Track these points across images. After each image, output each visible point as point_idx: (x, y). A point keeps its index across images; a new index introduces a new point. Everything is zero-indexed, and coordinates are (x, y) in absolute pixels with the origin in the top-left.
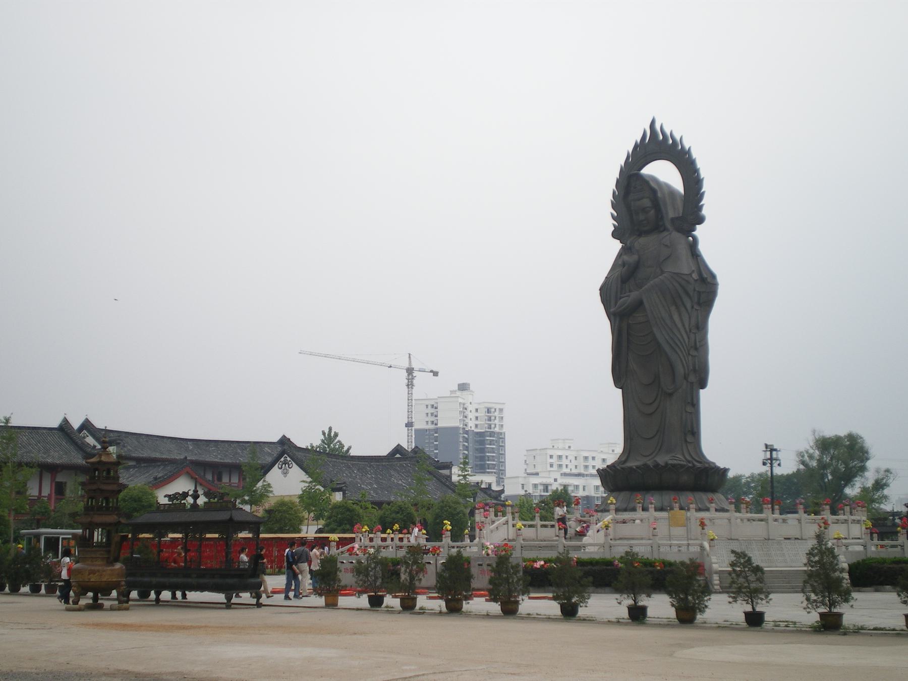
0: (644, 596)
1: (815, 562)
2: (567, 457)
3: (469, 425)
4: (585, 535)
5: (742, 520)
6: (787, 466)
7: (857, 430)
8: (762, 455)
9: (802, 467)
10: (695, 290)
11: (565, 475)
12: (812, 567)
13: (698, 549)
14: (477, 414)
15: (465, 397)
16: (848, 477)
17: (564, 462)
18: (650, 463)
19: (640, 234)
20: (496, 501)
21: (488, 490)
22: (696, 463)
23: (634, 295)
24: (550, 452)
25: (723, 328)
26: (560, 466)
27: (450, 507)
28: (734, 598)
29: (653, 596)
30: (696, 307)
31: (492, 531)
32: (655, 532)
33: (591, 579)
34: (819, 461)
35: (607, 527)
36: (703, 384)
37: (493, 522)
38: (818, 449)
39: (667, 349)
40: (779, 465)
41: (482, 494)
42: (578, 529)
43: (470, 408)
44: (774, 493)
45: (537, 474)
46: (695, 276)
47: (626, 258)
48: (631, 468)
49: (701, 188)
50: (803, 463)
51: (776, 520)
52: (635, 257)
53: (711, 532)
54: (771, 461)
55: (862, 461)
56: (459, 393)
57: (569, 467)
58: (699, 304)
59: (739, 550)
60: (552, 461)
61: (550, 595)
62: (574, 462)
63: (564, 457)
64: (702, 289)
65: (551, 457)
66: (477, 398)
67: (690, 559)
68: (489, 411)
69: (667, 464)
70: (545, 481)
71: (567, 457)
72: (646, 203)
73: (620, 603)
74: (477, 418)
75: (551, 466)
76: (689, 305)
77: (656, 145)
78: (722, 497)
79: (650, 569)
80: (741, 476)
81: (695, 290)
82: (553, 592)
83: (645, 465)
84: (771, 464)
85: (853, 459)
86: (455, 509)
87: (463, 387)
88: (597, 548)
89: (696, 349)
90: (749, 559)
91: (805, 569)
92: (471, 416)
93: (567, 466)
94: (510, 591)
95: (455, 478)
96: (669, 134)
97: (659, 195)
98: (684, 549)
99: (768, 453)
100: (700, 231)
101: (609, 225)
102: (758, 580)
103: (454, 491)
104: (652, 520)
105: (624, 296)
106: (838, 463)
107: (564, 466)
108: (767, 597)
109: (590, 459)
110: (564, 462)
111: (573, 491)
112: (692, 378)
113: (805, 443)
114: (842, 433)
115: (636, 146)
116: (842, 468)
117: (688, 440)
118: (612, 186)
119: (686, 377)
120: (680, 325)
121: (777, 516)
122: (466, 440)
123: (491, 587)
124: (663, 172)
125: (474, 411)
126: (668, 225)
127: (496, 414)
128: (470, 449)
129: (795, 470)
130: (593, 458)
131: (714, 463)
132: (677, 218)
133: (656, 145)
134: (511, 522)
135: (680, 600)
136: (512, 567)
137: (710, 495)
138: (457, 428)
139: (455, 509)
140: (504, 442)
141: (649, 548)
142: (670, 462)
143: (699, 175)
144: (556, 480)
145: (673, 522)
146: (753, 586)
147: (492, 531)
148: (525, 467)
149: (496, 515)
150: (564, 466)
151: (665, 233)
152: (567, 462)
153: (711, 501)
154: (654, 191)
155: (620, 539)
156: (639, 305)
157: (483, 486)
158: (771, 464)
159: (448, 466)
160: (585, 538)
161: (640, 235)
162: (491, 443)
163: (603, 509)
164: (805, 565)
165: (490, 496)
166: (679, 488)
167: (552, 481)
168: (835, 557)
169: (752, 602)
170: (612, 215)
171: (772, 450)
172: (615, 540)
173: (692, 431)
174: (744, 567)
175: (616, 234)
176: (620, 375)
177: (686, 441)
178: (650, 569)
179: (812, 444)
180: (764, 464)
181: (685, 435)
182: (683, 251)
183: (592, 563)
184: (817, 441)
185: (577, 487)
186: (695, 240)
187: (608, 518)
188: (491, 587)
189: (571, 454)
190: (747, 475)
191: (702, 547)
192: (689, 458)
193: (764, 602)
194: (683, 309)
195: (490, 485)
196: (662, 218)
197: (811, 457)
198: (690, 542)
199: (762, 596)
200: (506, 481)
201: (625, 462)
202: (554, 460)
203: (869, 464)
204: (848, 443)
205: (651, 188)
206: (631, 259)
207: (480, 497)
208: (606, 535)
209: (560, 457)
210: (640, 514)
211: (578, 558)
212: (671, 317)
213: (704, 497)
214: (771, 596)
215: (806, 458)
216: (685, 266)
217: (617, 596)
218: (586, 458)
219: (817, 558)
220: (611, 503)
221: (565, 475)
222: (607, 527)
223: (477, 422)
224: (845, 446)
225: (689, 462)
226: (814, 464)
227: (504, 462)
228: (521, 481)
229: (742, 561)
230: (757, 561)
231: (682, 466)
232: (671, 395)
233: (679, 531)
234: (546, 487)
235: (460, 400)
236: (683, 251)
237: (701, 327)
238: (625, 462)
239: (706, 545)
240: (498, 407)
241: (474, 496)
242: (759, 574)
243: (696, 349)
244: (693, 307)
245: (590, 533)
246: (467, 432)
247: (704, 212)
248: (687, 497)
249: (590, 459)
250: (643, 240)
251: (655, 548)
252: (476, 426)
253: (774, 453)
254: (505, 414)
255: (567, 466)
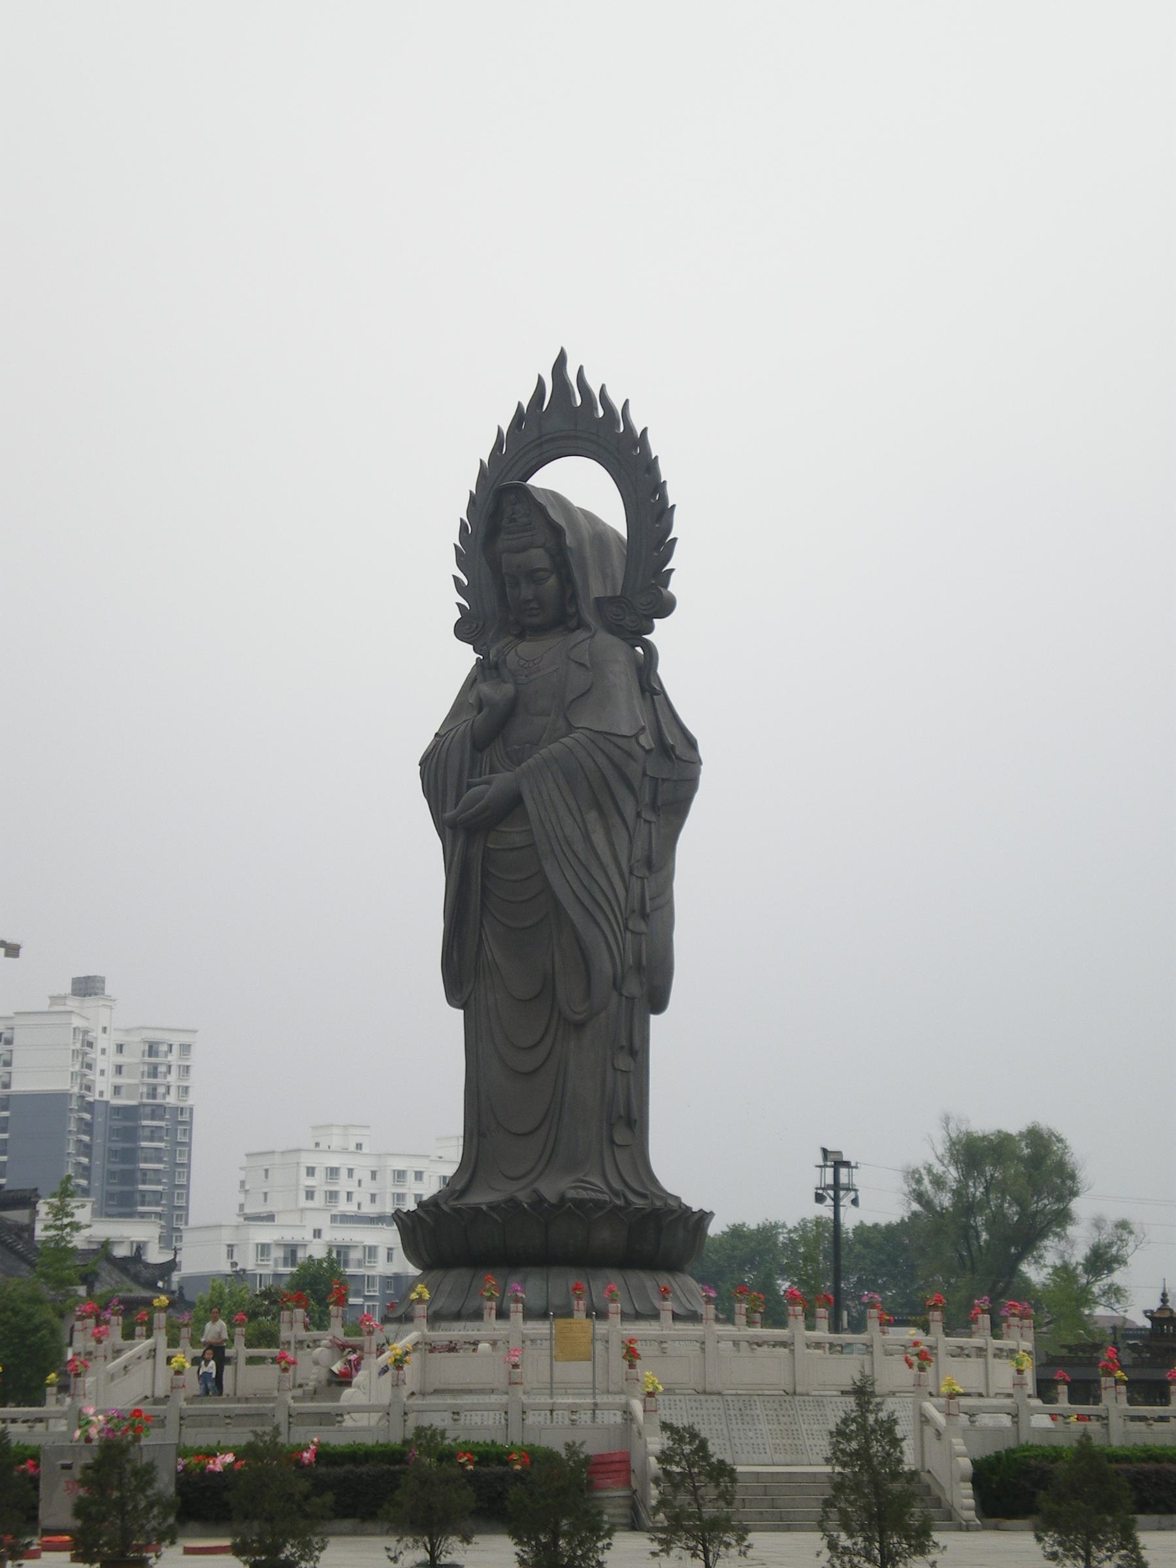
0: (454, 1541)
1: (851, 1455)
2: (351, 1172)
3: (99, 1087)
4: (349, 1384)
5: (736, 1343)
6: (880, 1203)
7: (1049, 1121)
8: (815, 1177)
9: (916, 1207)
10: (644, 774)
11: (345, 1218)
12: (844, 1465)
13: (617, 1418)
14: (120, 1060)
15: (90, 1014)
16: (1027, 1236)
17: (343, 1185)
18: (523, 1197)
19: (523, 633)
20: (137, 1294)
21: (133, 1265)
22: (632, 1197)
23: (502, 780)
24: (308, 1160)
25: (713, 869)
26: (333, 1196)
27: (16, 1312)
28: (661, 1541)
29: (475, 1539)
30: (647, 815)
31: (112, 1377)
32: (524, 1375)
33: (329, 1498)
34: (959, 1194)
35: (399, 1363)
36: (658, 1003)
37: (118, 1352)
38: (955, 1160)
39: (575, 914)
40: (855, 1202)
41: (116, 1275)
42: (337, 1367)
43: (102, 1041)
44: (832, 1275)
45: (270, 1217)
46: (646, 741)
47: (485, 688)
48: (476, 1209)
49: (668, 530)
50: (920, 1197)
51: (818, 1345)
52: (509, 689)
53: (648, 1375)
54: (835, 1191)
55: (1060, 1198)
56: (73, 1004)
57: (356, 1198)
58: (654, 807)
59: (678, 1423)
60: (310, 1182)
61: (227, 1542)
62: (369, 1186)
63: (343, 1173)
64: (660, 773)
65: (311, 1171)
66: (122, 1018)
67: (569, 1447)
68: (152, 1049)
69: (563, 1199)
70: (289, 1236)
71: (351, 1172)
72: (538, 558)
73: (394, 1559)
74: (119, 1069)
75: (310, 1195)
76: (629, 810)
77: (565, 417)
78: (692, 1283)
79: (498, 1469)
80: (776, 1226)
81: (644, 774)
82: (234, 1535)
83: (512, 1201)
84: (836, 1200)
85: (1038, 1193)
86: (30, 1317)
87: (87, 987)
88: (375, 1417)
89: (644, 916)
90: (703, 1445)
91: (828, 1469)
92: (104, 1062)
93: (349, 1195)
94: (127, 1534)
95: (40, 1233)
96: (596, 393)
97: (569, 540)
98: (585, 1417)
99: (830, 1172)
100: (662, 633)
101: (448, 606)
102: (721, 1496)
103: (32, 1265)
104: (515, 1343)
105: (483, 783)
106: (1006, 1194)
107: (343, 1197)
108: (741, 1539)
109: (411, 1176)
110: (343, 1185)
111: (360, 1263)
112: (633, 987)
113: (928, 1150)
114: (1014, 1126)
115: (520, 416)
116: (1012, 1211)
117: (618, 1139)
118: (460, 510)
119: (617, 985)
120: (607, 858)
121: (822, 1333)
122: (88, 1127)
123: (79, 1523)
124: (579, 484)
125: (111, 1049)
126: (589, 617)
127: (173, 1058)
128: (97, 1151)
129: (906, 1215)
130: (419, 1175)
131: (677, 1199)
132: (612, 600)
133: (565, 417)
134: (163, 1351)
135: (540, 1549)
136: (136, 1473)
137: (664, 1279)
138: (63, 1097)
139: (30, 1317)
140: (188, 1132)
141: (499, 1416)
142: (571, 1194)
143: (664, 498)
144: (317, 1233)
145: (562, 1350)
146: (709, 1511)
147: (112, 1377)
148: (241, 1198)
149: (129, 1335)
150: (343, 1197)
151: (580, 635)
152: (351, 1186)
153: (664, 1294)
154: (557, 531)
155: (436, 1392)
156: (513, 804)
157: (120, 1252)
158: (836, 1200)
159: (26, 1200)
160: (348, 1392)
161: (521, 636)
162: (154, 1134)
163: (398, 1314)
164: (828, 1461)
165: (135, 1278)
166: (588, 1260)
167: (309, 1236)
168: (896, 1442)
169: (706, 1552)
170: (456, 578)
171: (840, 1164)
172: (423, 1394)
173: (627, 1117)
174: (691, 1466)
175: (463, 631)
176: (462, 974)
177: (612, 1142)
178: (498, 1469)
179: (941, 1150)
180: (819, 1198)
181: (611, 1126)
182: (620, 677)
183: (355, 1456)
184: (953, 1143)
185: (371, 1251)
186: (651, 653)
187: (410, 1336)
188: (79, 1523)
189: (362, 1165)
190: (790, 1226)
191: (627, 1412)
192: (617, 1185)
193: (733, 1551)
194: (615, 819)
195: (140, 1248)
196: (574, 596)
197: (938, 1182)
198: (599, 1399)
199: (730, 1538)
200: (187, 1237)
201: (463, 1192)
202: (318, 1182)
203: (1077, 1206)
204: (1026, 1151)
205: (552, 523)
206: (497, 692)
207: (109, 1282)
208: (396, 1384)
209: (333, 1172)
210: (491, 1327)
211: (319, 1445)
212: (587, 837)
213: (649, 1282)
214: (752, 1537)
215: (927, 1185)
216: (624, 716)
217: (391, 1541)
218: (400, 1175)
219: (854, 1445)
220: (420, 1300)
221: (345, 1218)
222: (399, 1363)
223: (119, 1081)
224: (1020, 1159)
225: (616, 1194)
226: (945, 1200)
227: (186, 1187)
228: (227, 1237)
229: (687, 1449)
230: (718, 1450)
231: (599, 1205)
232: (580, 1026)
233: (577, 1371)
234: (292, 1251)
235: (76, 1022)
236: (620, 677)
237: (657, 864)
238: (463, 1192)
239: (637, 1406)
240: (177, 1039)
241: (89, 1279)
242: (724, 1481)
243: (644, 916)
244: (639, 815)
245: (359, 1378)
246: (90, 1107)
247: (674, 587)
248: (611, 1286)
249: (411, 1176)
250: (526, 648)
251: (515, 1416)
252: (117, 1090)
253: (843, 1171)
254: (196, 1060)
255: (349, 1195)
